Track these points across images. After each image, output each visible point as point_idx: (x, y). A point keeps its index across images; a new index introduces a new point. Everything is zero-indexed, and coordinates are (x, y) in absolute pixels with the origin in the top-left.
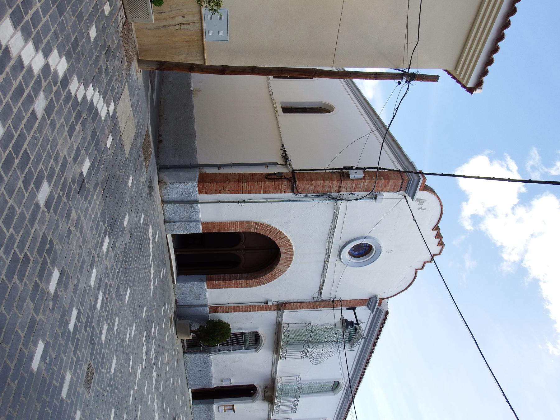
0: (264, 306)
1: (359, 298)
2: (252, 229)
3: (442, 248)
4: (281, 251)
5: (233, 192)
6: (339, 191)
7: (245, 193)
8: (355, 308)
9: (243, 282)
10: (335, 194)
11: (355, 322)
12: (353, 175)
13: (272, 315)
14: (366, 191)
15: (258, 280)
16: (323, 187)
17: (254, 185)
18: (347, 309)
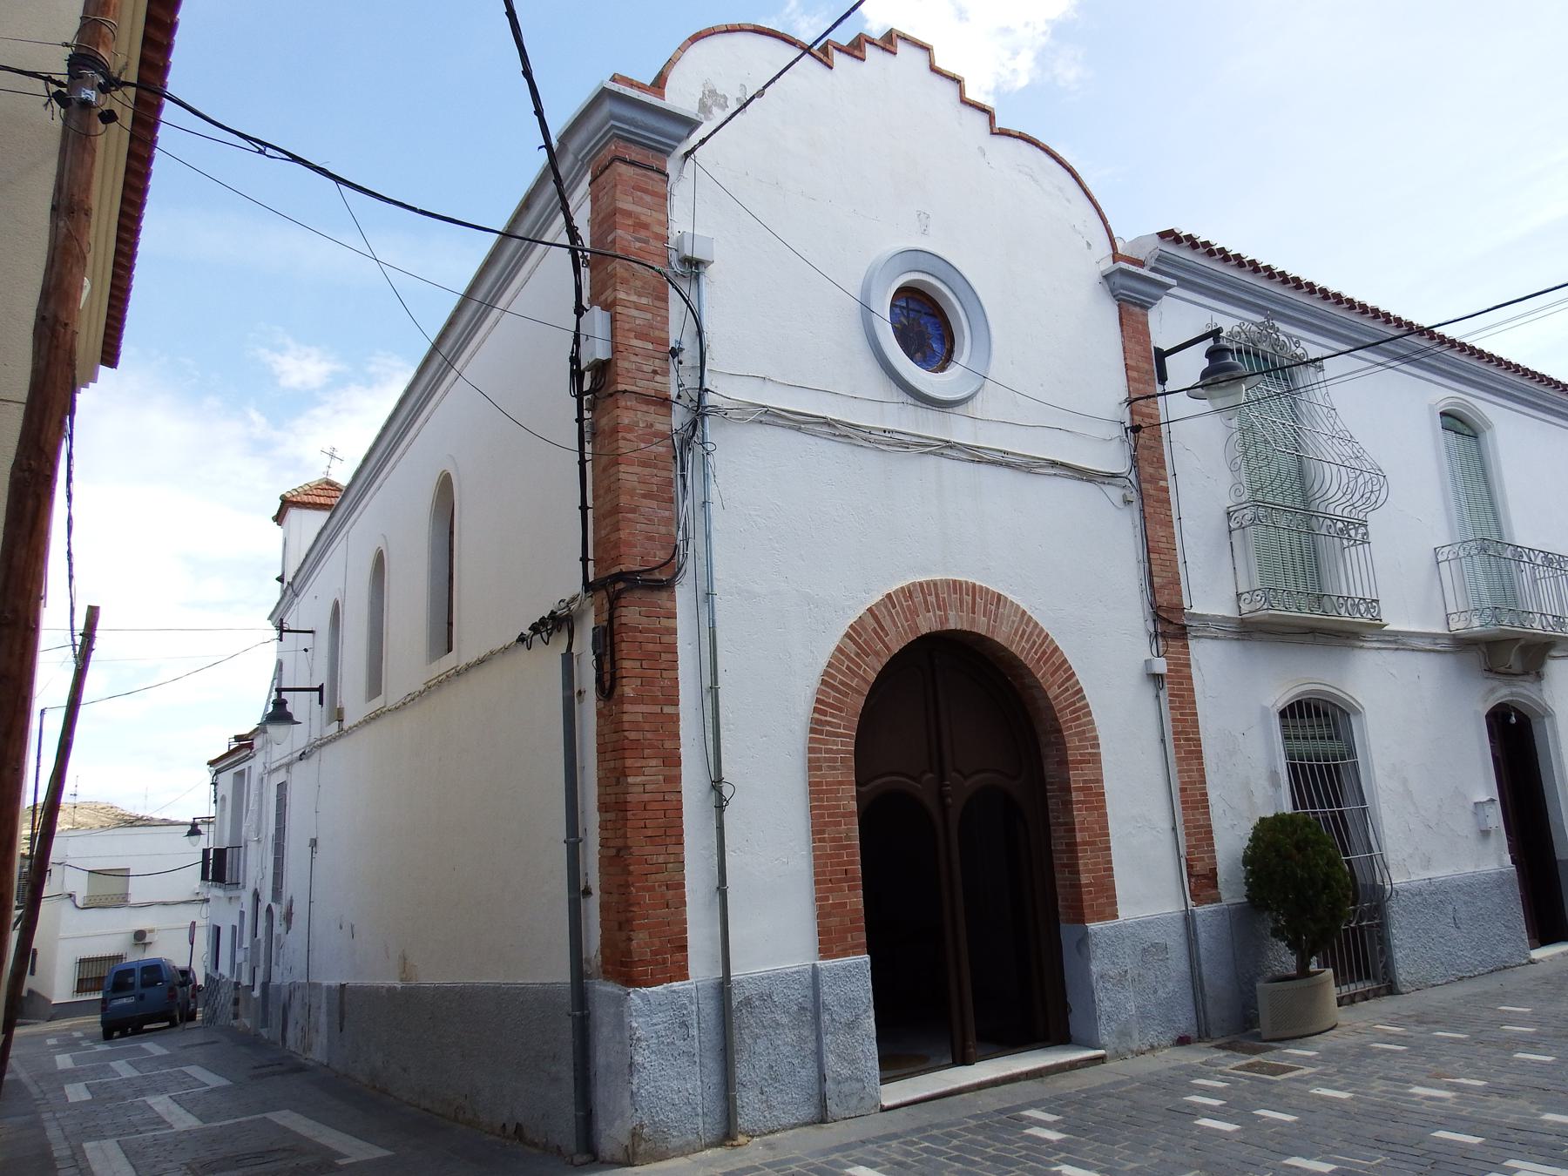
2: (844, 745)
4: (936, 627)
5: (672, 832)
6: (664, 402)
7: (678, 778)
8: (1157, 350)
9: (1076, 777)
10: (679, 418)
11: (1210, 342)
12: (597, 349)
14: (666, 300)
15: (1065, 717)
16: (644, 464)
18: (1163, 379)
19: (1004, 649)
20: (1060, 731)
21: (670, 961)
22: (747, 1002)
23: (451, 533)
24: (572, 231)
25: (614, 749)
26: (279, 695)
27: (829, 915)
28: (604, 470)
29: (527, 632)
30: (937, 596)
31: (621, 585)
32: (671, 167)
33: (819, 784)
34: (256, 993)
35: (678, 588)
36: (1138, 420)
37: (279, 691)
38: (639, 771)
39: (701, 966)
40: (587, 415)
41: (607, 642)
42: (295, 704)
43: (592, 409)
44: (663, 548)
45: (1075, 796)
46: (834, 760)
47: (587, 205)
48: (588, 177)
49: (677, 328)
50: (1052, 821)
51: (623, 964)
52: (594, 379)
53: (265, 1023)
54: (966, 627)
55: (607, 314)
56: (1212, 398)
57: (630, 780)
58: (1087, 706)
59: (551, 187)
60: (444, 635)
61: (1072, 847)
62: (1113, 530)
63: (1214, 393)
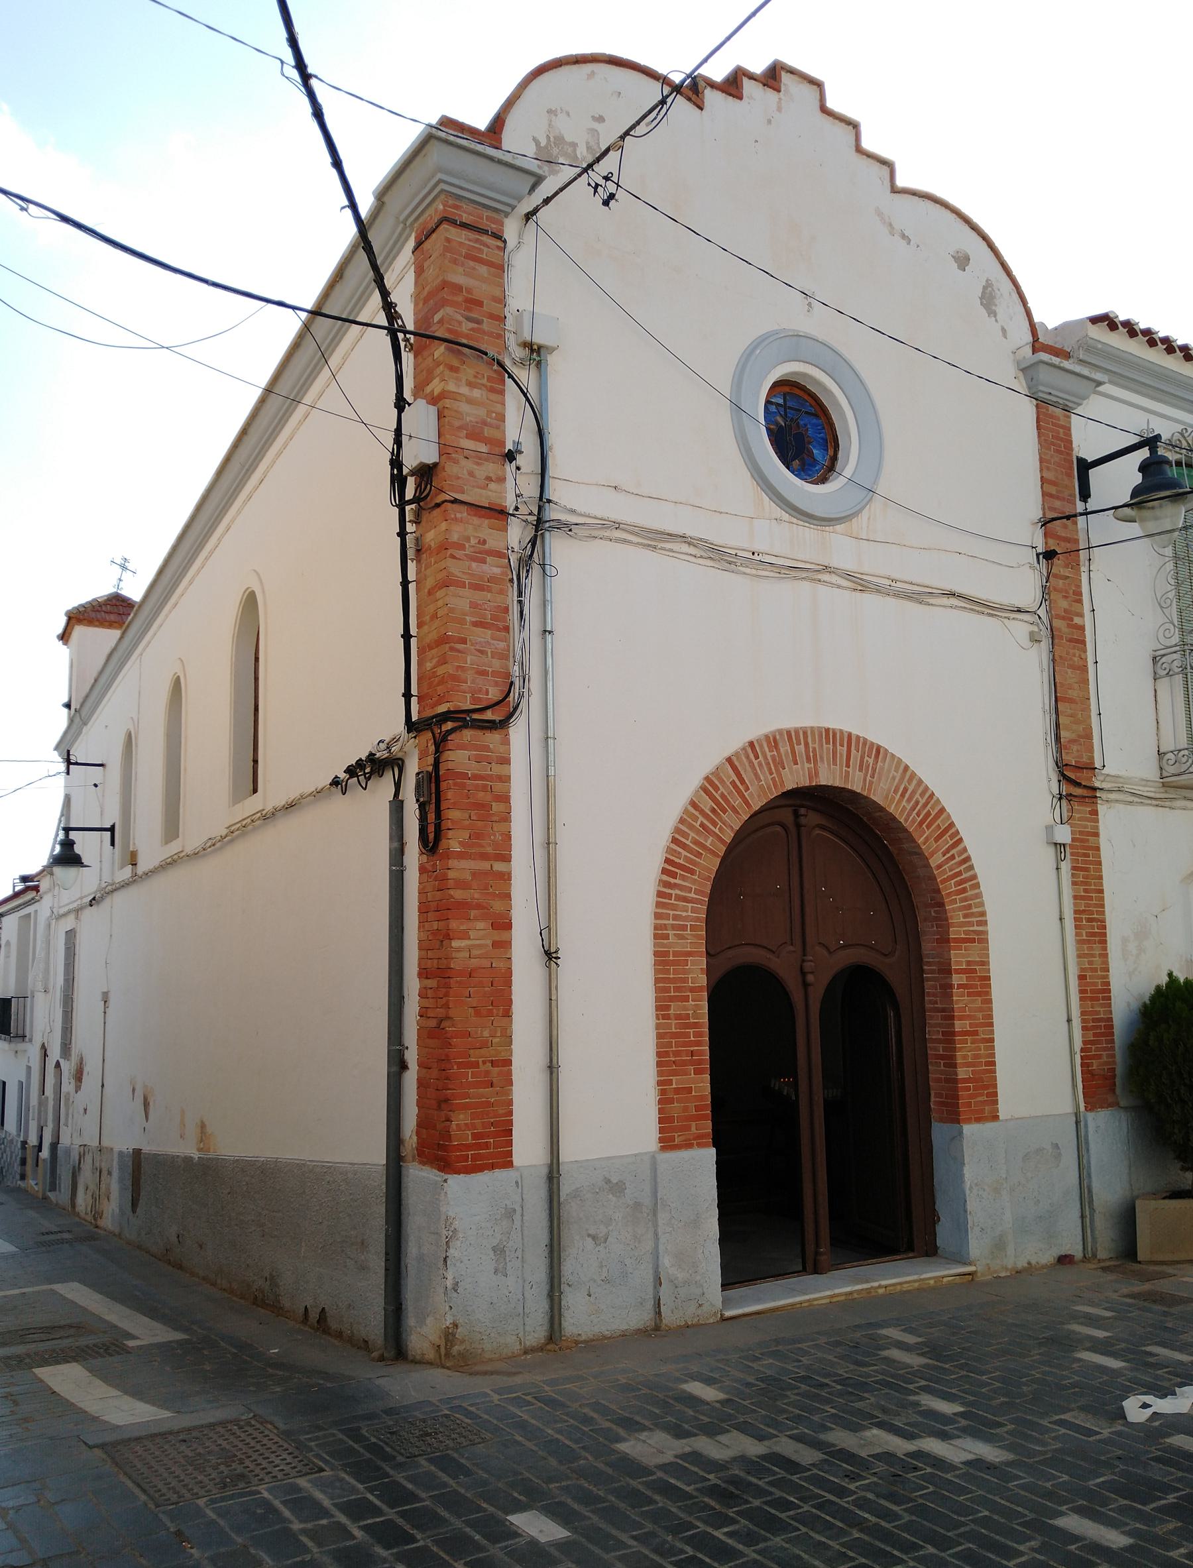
0: (1082, 860)
1: (1036, 446)
2: (695, 912)
3: (792, 71)
4: (805, 782)
5: (499, 1001)
6: (500, 514)
7: (507, 944)
8: (1081, 461)
9: (958, 958)
10: (516, 534)
11: (1144, 453)
12: (417, 453)
13: (1115, 823)
14: (502, 392)
15: (949, 888)
16: (477, 587)
17: (463, 907)
18: (1085, 495)
19: (882, 809)
20: (941, 905)
21: (493, 1149)
22: (576, 1194)
23: (257, 659)
24: (389, 307)
25: (441, 911)
26: (67, 835)
27: (671, 1101)
28: (430, 593)
29: (343, 776)
30: (807, 744)
31: (449, 725)
32: (511, 229)
33: (666, 954)
34: (45, 1153)
35: (512, 730)
36: (1053, 546)
37: (67, 830)
38: (465, 936)
39: (528, 1146)
40: (410, 528)
41: (432, 786)
42: (84, 844)
43: (417, 521)
44: (496, 684)
45: (956, 979)
46: (684, 928)
47: (411, 277)
48: (411, 244)
49: (516, 428)
50: (928, 1006)
51: (440, 1147)
52: (418, 486)
53: (53, 1187)
54: (837, 784)
55: (433, 410)
56: (1142, 520)
57: (455, 944)
58: (975, 877)
59: (362, 255)
60: (250, 778)
61: (949, 1036)
62: (1018, 669)
63: (1146, 513)
